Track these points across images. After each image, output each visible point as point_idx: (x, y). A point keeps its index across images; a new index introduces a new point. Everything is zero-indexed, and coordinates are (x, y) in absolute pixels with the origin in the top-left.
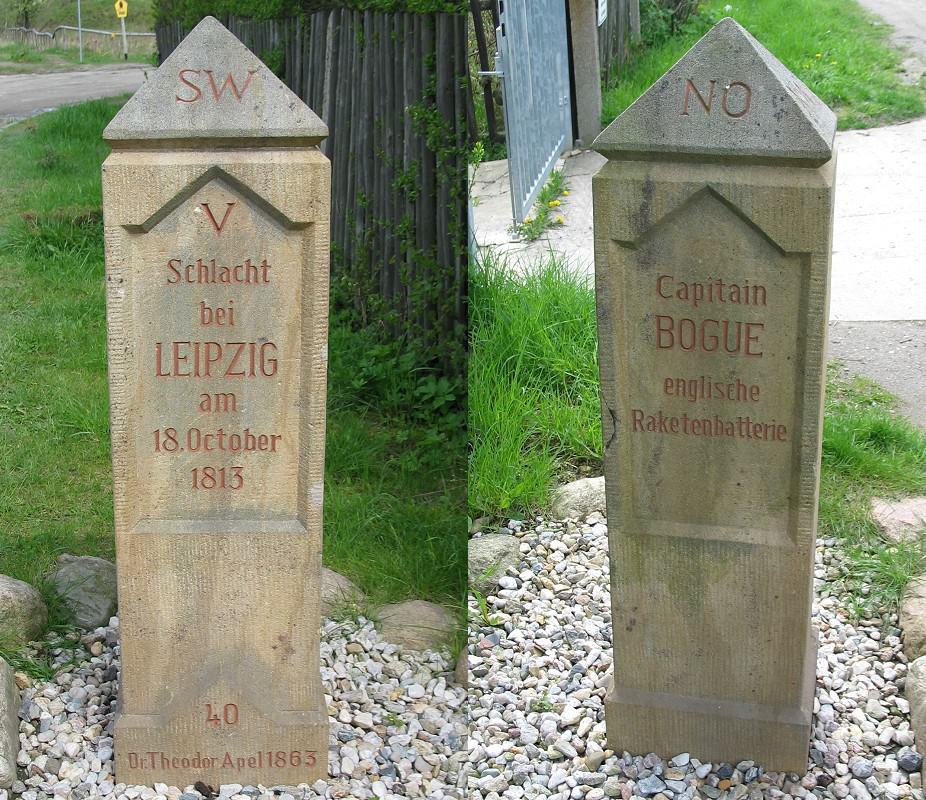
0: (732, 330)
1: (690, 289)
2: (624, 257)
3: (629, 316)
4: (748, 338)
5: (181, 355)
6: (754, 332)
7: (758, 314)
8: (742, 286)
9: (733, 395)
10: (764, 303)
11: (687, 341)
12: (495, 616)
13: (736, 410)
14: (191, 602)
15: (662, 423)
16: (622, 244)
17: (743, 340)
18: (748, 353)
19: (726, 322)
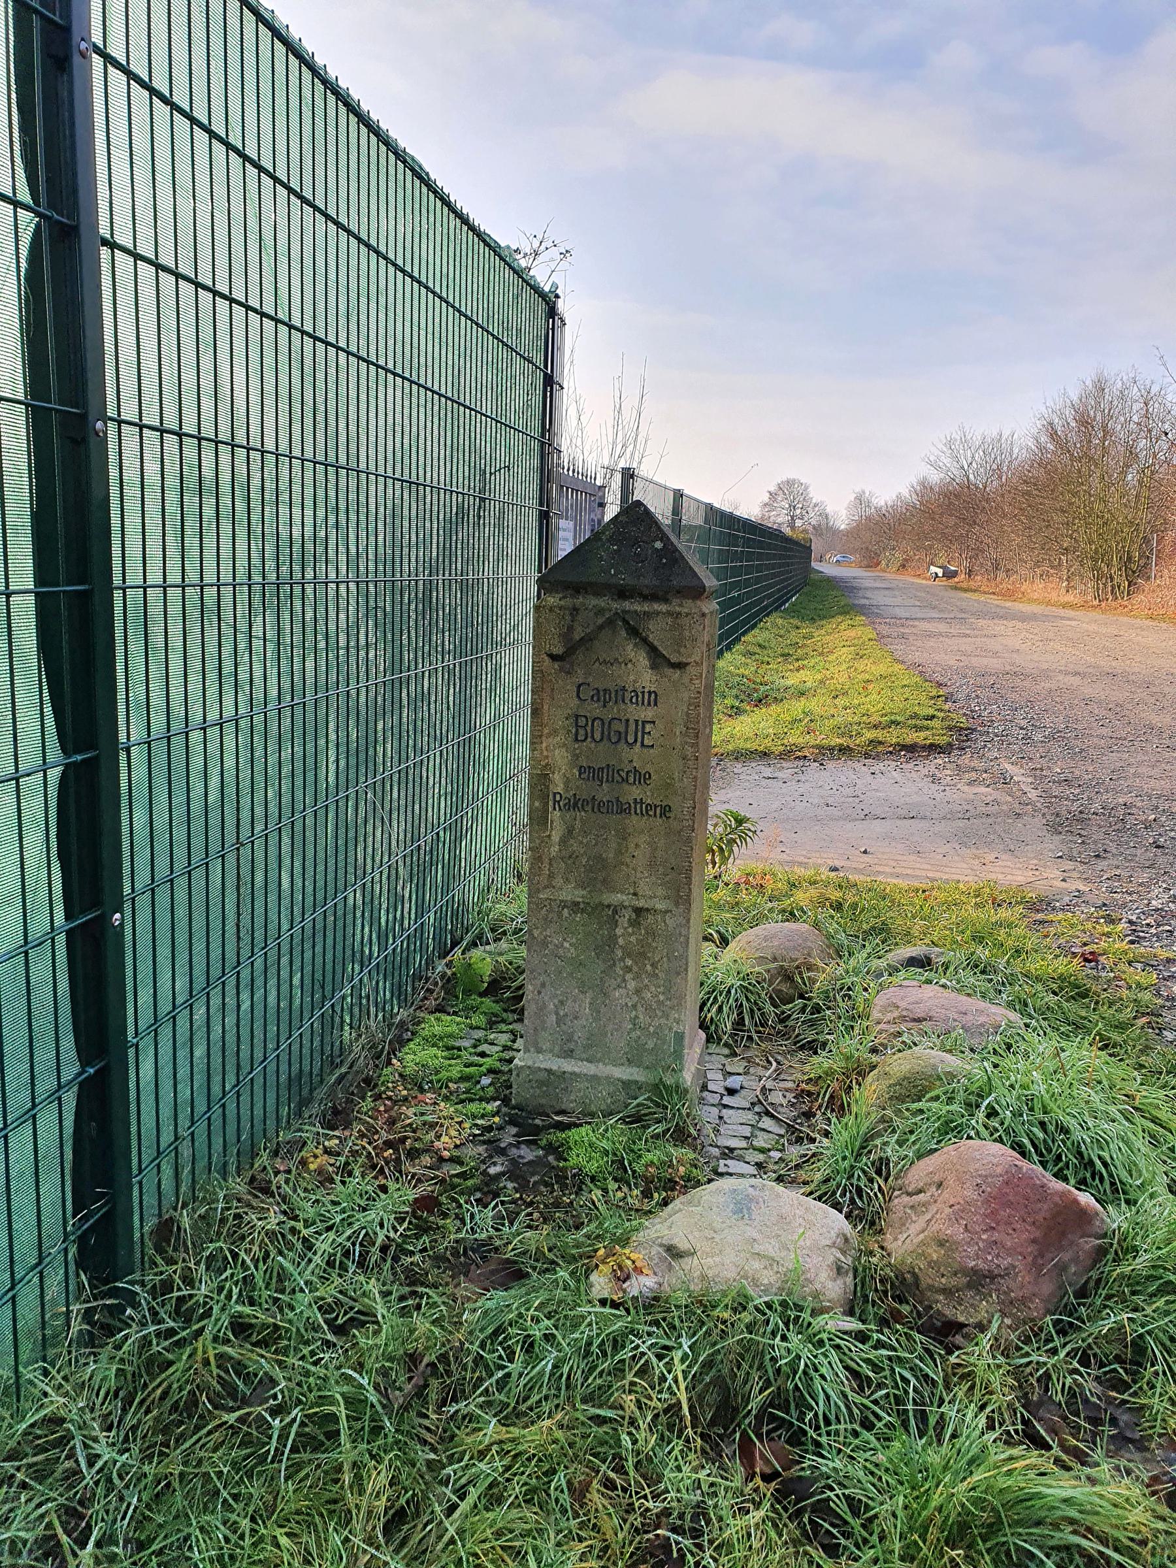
0: (632, 727)
1: (602, 693)
2: (556, 666)
3: (961, 686)
4: (644, 733)
5: (647, 730)
6: (648, 728)
7: (648, 713)
8: (639, 690)
9: (631, 780)
10: (656, 704)
11: (597, 736)
12: (422, 1015)
13: (634, 792)
14: (849, 1279)
15: (576, 804)
16: (553, 657)
17: (640, 734)
18: (643, 745)
19: (628, 721)
